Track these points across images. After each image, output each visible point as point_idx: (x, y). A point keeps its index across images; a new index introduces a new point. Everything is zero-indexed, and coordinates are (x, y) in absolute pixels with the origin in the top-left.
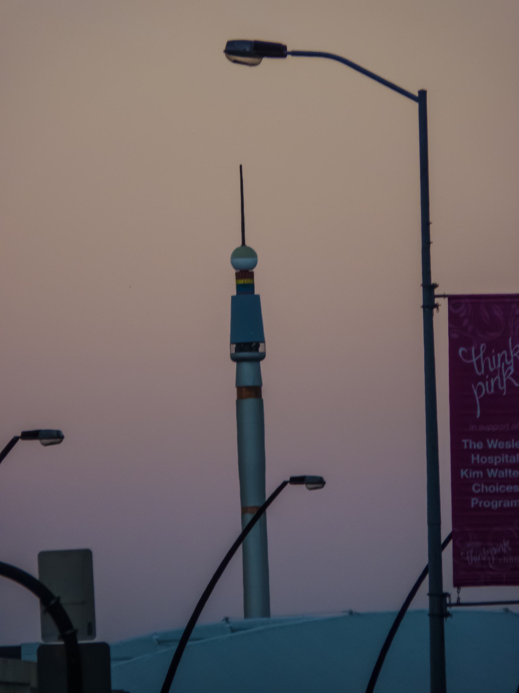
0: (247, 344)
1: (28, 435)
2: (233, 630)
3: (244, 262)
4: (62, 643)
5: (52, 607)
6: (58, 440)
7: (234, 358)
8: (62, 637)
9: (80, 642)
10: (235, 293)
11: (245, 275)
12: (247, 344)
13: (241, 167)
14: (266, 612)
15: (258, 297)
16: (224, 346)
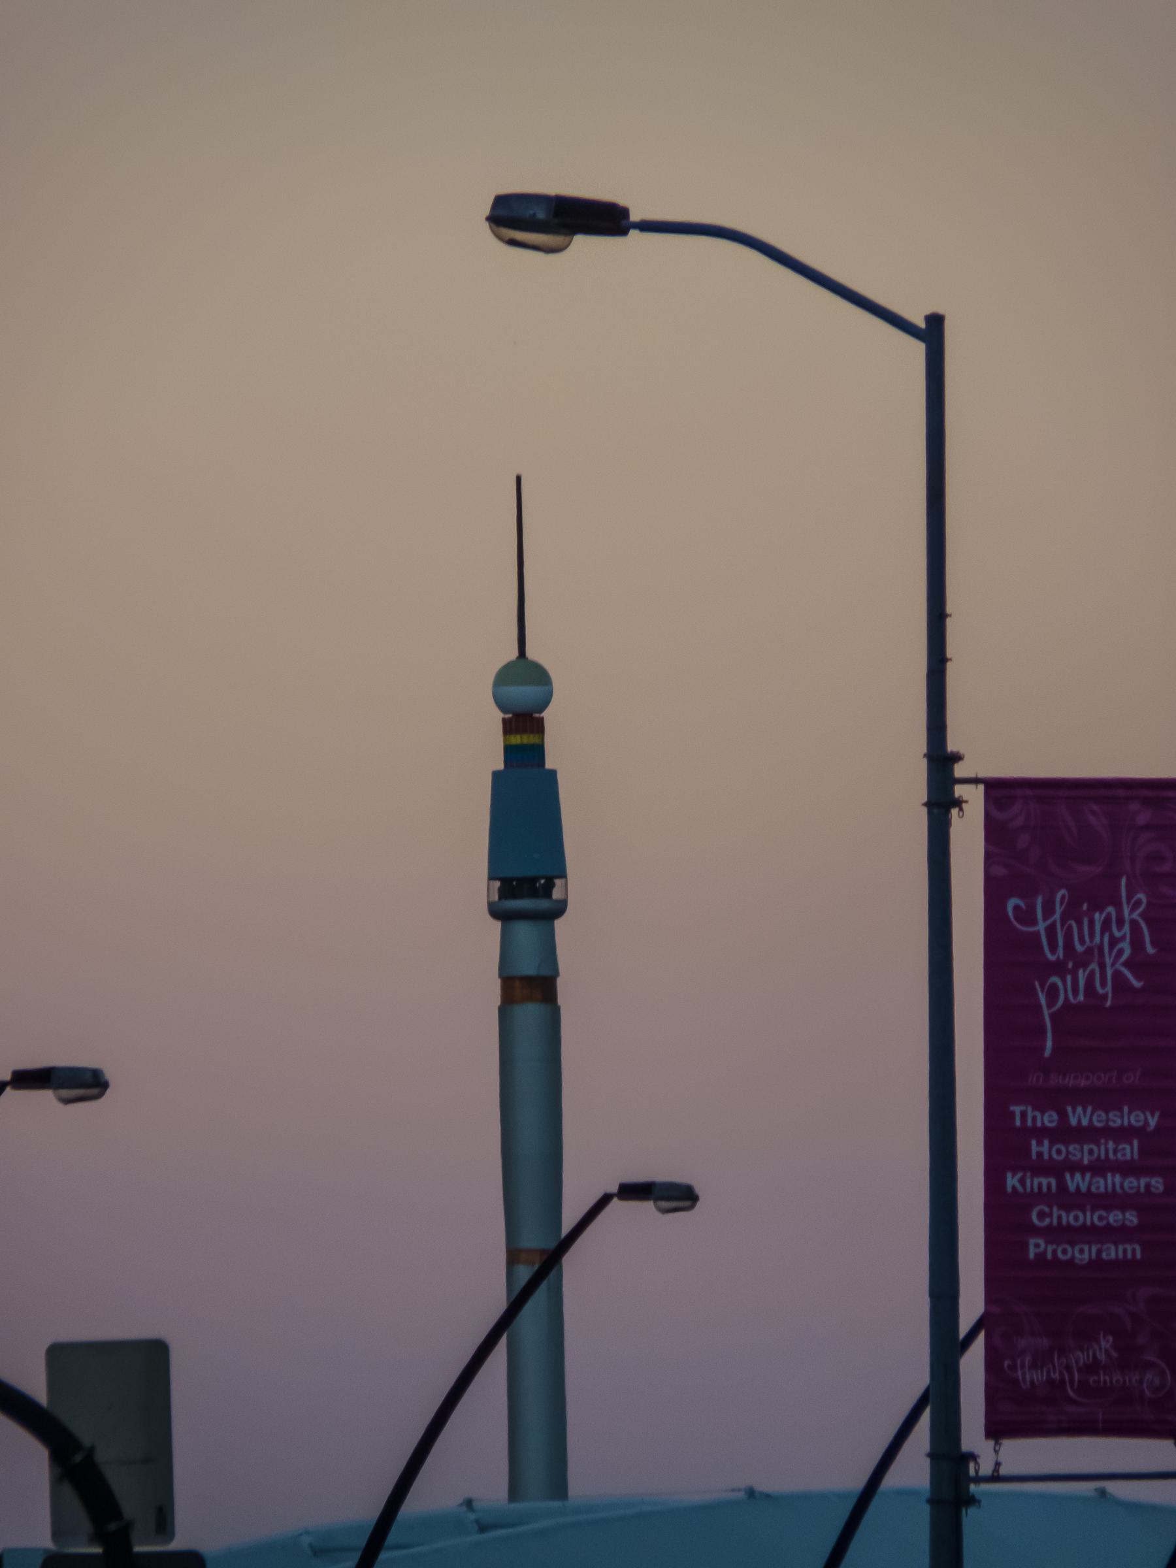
0: (527, 879)
2: (483, 1528)
3: (523, 693)
4: (97, 1550)
5: (75, 1468)
6: (95, 1091)
8: (98, 1536)
9: (138, 1549)
10: (500, 766)
11: (524, 724)
12: (527, 879)
13: (519, 479)
14: (558, 1486)
15: (553, 774)
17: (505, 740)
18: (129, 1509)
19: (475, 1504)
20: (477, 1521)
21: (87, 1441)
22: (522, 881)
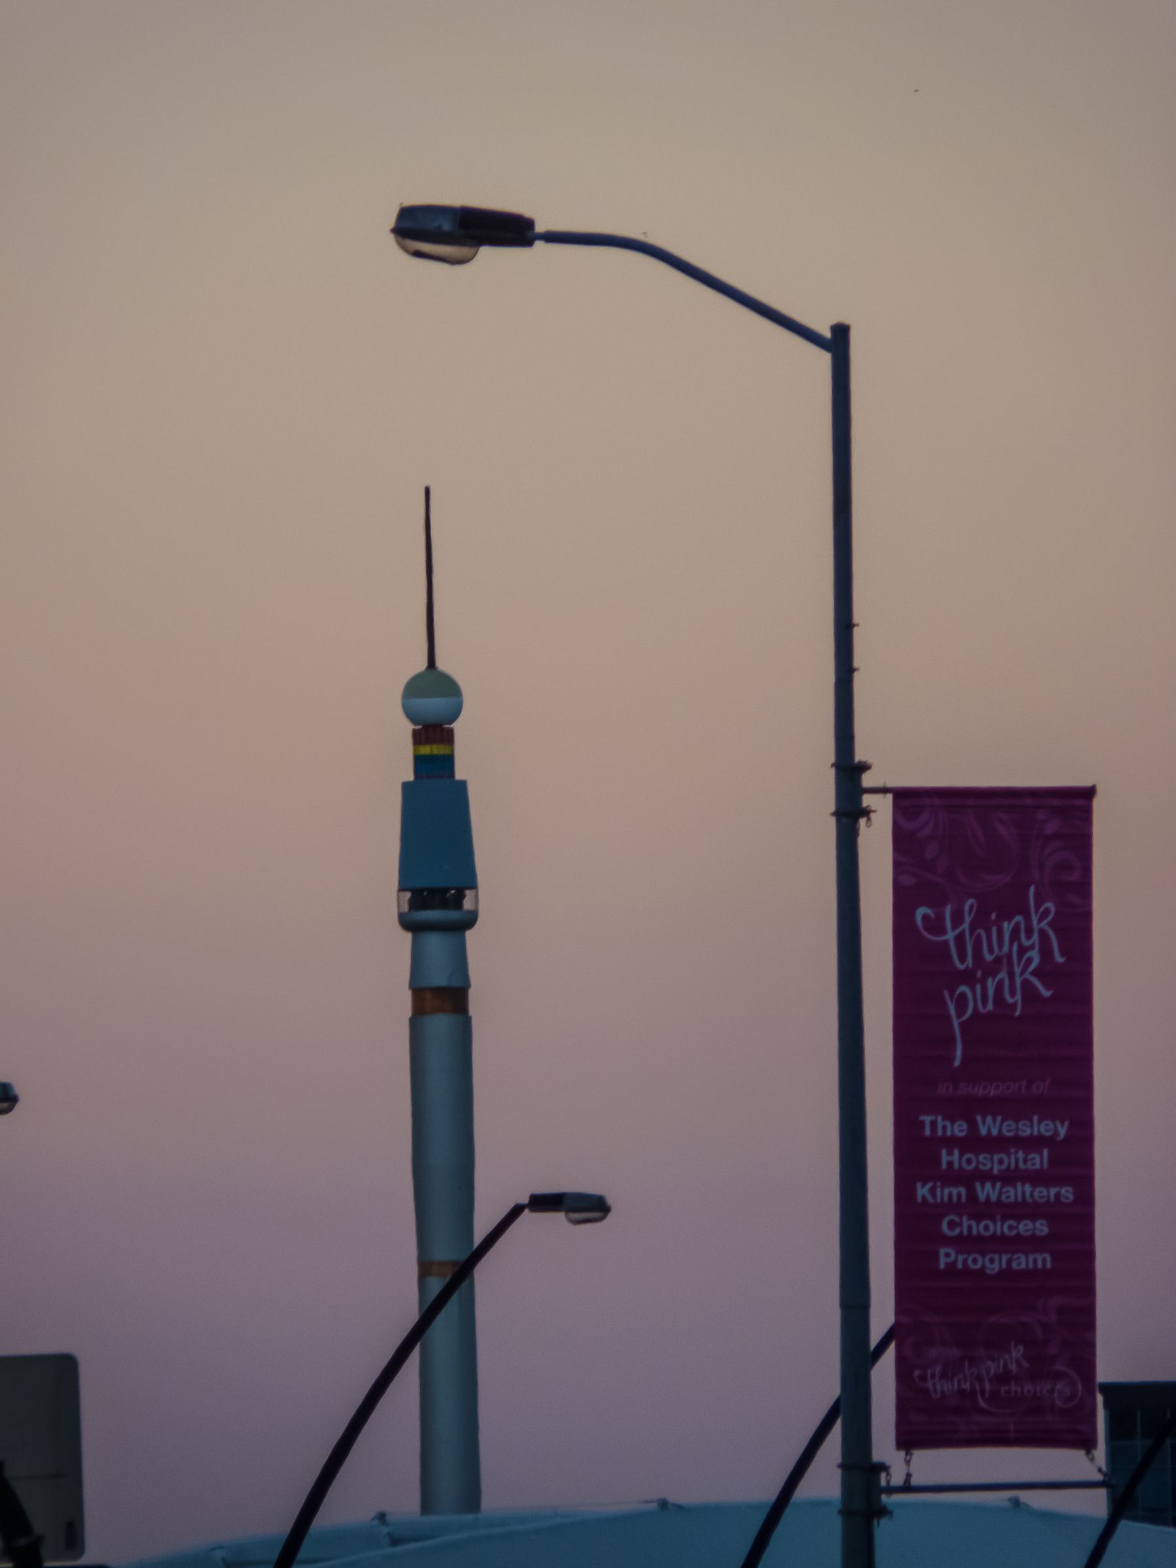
0: (437, 889)
2: (395, 1541)
3: (433, 705)
7: (406, 924)
9: (47, 1564)
10: (410, 777)
11: (433, 735)
12: (437, 889)
13: (427, 491)
14: (471, 1499)
15: (463, 785)
17: (415, 750)
19: (389, 1518)
20: (390, 1535)
22: (433, 891)
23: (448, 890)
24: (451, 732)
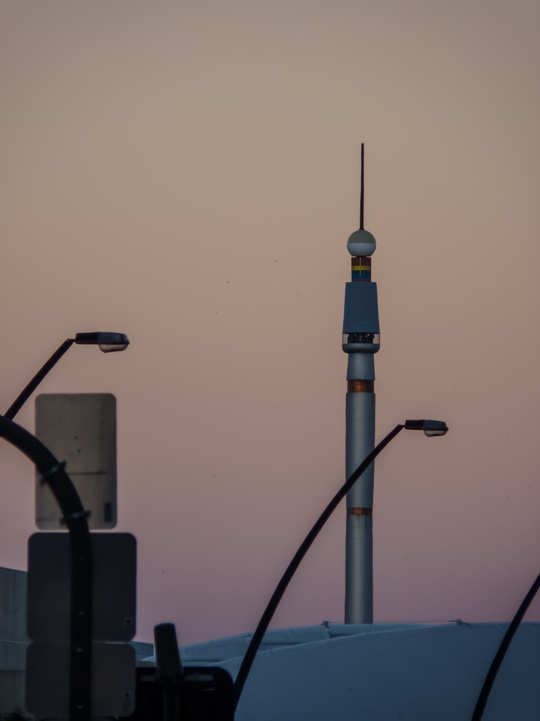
0: (361, 333)
1: (85, 338)
2: (332, 636)
3: (361, 247)
4: (66, 531)
5: (52, 475)
6: (121, 346)
7: (346, 349)
8: (66, 521)
9: (92, 531)
10: (350, 280)
11: (361, 262)
12: (361, 333)
13: (363, 145)
14: (368, 617)
15: (375, 284)
16: (338, 338)
17: (352, 268)
18: (87, 505)
19: (329, 624)
20: (329, 633)
21: (60, 460)
22: (358, 334)
23: (366, 334)
24: (370, 260)
